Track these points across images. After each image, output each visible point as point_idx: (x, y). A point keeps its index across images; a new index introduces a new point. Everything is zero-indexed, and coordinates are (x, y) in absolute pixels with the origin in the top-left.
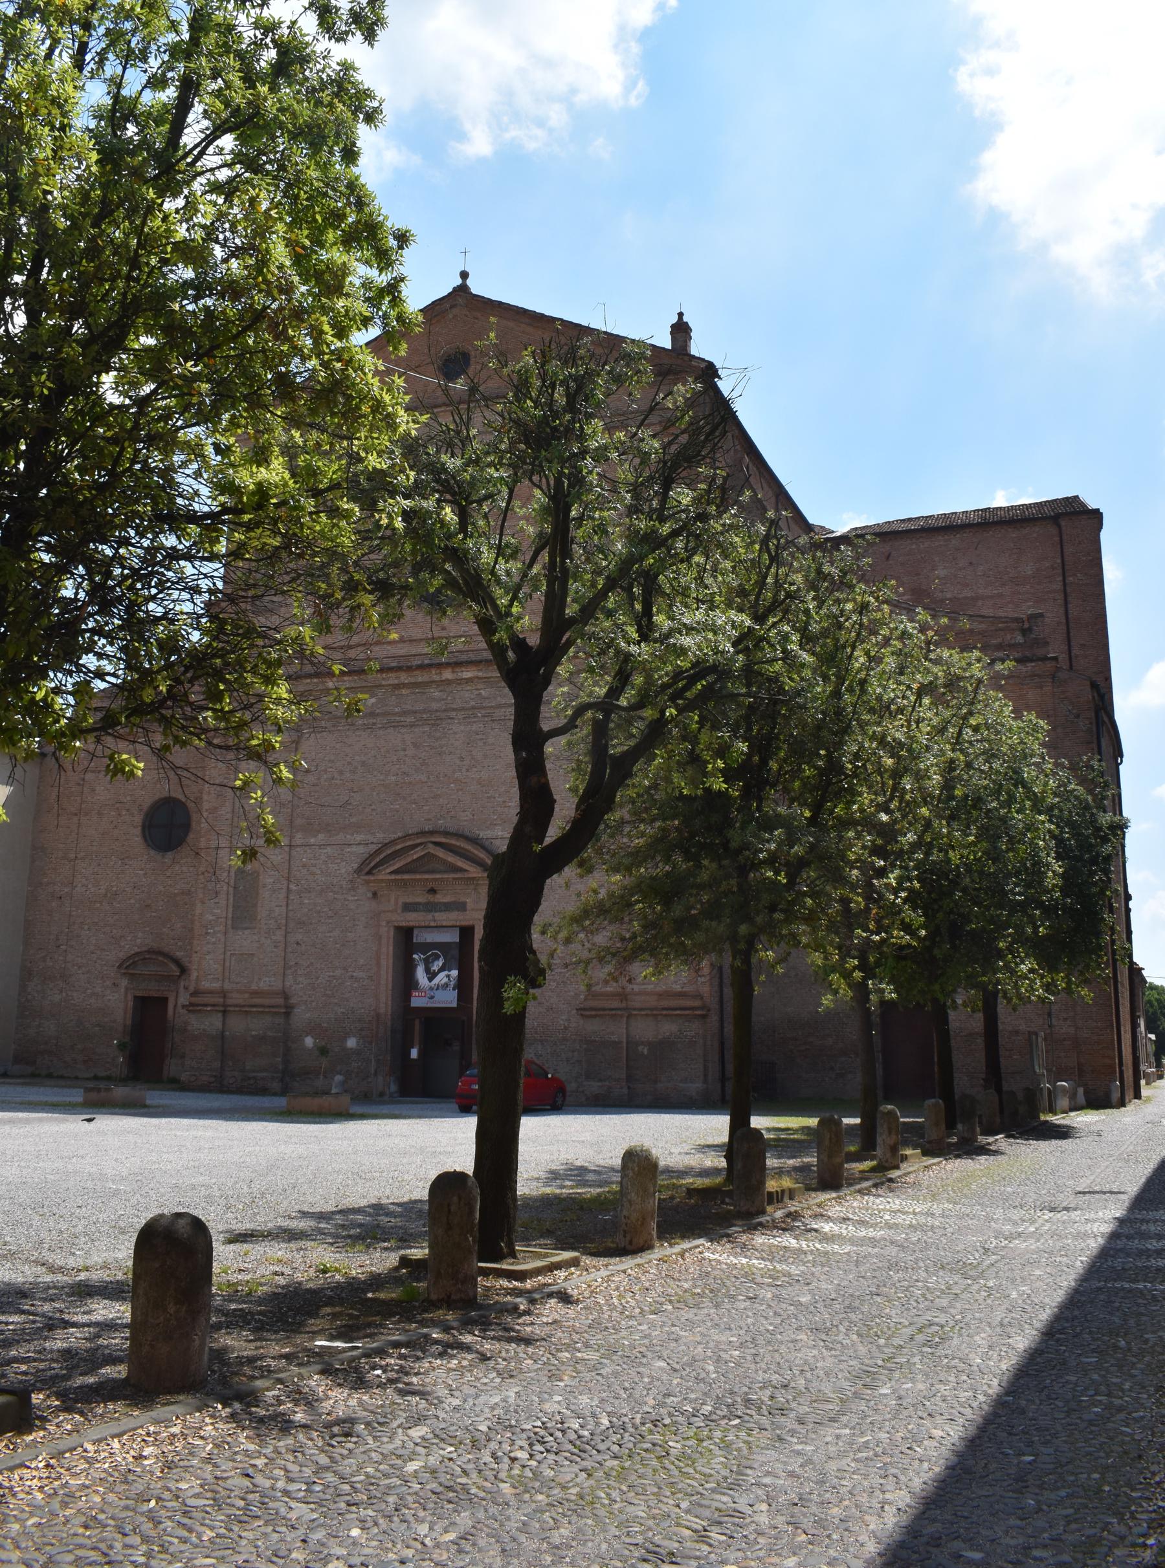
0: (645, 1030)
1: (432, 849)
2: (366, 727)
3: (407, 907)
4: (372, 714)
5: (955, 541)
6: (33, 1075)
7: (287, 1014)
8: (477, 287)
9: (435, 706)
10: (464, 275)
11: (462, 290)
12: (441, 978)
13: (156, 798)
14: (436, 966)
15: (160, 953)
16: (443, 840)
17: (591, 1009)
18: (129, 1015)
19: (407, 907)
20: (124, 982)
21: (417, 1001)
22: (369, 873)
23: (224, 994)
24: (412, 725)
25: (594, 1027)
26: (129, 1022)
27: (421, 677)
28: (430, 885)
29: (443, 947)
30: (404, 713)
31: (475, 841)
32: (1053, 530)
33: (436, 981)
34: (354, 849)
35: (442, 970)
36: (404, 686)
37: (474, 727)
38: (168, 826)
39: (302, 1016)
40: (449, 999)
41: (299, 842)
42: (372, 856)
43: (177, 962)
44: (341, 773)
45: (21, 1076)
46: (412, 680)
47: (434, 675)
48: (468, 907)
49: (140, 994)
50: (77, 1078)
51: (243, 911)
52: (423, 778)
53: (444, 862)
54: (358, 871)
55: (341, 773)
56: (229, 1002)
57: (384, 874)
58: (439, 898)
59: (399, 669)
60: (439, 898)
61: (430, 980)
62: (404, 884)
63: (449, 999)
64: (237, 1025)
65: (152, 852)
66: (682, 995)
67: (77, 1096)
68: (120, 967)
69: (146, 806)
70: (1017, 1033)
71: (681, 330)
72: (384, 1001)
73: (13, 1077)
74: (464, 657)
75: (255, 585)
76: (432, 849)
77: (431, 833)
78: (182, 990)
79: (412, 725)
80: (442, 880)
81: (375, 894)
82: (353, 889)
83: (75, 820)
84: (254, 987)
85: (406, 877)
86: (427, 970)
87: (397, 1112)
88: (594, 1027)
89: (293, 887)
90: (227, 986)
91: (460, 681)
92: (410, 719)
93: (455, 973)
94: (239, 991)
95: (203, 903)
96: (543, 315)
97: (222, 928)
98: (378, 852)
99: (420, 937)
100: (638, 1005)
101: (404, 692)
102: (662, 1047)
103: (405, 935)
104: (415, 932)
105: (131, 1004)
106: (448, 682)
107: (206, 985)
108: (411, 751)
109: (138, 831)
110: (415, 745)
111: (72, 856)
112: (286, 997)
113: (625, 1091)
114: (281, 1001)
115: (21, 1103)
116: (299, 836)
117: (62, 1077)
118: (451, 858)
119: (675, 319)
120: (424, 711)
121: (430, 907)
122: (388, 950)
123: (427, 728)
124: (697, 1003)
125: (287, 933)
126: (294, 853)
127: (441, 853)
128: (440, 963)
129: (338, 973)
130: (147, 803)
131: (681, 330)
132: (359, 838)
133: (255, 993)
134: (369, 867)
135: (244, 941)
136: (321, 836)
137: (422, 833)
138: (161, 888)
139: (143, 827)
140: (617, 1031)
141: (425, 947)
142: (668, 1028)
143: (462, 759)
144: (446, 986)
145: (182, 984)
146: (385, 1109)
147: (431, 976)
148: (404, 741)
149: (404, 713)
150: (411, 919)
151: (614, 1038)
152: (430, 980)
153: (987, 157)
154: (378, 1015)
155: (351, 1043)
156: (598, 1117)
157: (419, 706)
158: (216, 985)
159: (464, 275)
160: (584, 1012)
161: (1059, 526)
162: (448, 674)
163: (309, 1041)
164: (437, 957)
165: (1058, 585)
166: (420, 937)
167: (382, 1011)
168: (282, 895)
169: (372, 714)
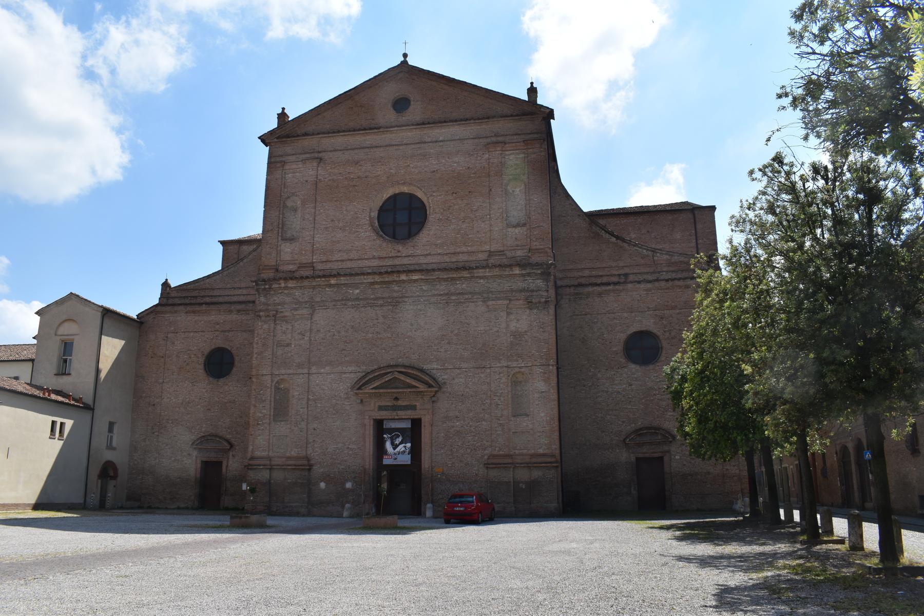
0: (523, 475)
1: (397, 375)
2: (353, 307)
3: (381, 408)
4: (357, 299)
5: (640, 220)
6: (139, 507)
7: (309, 470)
8: (411, 61)
9: (395, 295)
10: (405, 55)
11: (404, 63)
12: (401, 448)
13: (213, 347)
14: (397, 442)
15: (216, 436)
16: (403, 370)
17: (493, 464)
18: (199, 470)
19: (381, 408)
20: (195, 453)
21: (387, 461)
22: (359, 388)
23: (269, 458)
24: (381, 306)
25: (494, 474)
26: (198, 476)
27: (387, 278)
28: (395, 395)
29: (402, 431)
30: (377, 299)
31: (422, 370)
32: (690, 216)
33: (398, 449)
34: (348, 375)
35: (401, 443)
36: (377, 283)
37: (419, 307)
38: (219, 364)
39: (318, 470)
40: (406, 459)
41: (314, 371)
42: (361, 379)
43: (228, 441)
44: (339, 332)
45: (132, 508)
46: (381, 280)
47: (395, 277)
48: (418, 407)
49: (204, 459)
50: (166, 508)
51: (281, 410)
52: (389, 335)
53: (404, 382)
54: (352, 388)
55: (339, 332)
56: (273, 463)
57: (368, 389)
58: (400, 403)
59: (374, 273)
61: (394, 449)
62: (380, 396)
63: (406, 459)
64: (278, 476)
65: (211, 379)
66: (543, 455)
67: (226, 520)
68: (193, 444)
69: (206, 352)
70: (709, 473)
71: (532, 91)
72: (368, 461)
73: (127, 509)
74: (412, 268)
75: (338, 242)
76: (397, 375)
77: (396, 366)
78: (231, 456)
79: (381, 306)
80: (403, 392)
81: (362, 401)
82: (348, 398)
83: (162, 360)
84: (288, 454)
85: (381, 391)
86: (392, 444)
87: (418, 525)
88: (494, 474)
89: (311, 397)
90: (271, 454)
91: (411, 281)
92: (381, 302)
93: (409, 445)
94: (279, 457)
95: (255, 406)
96: (454, 79)
97: (267, 421)
98: (363, 377)
99: (387, 425)
100: (519, 461)
101: (376, 286)
102: (533, 485)
103: (379, 424)
104: (385, 422)
105: (199, 466)
106: (404, 281)
107: (258, 454)
108: (381, 320)
109: (202, 367)
110: (383, 316)
111: (161, 381)
112: (309, 460)
113: (513, 509)
114: (305, 462)
115: (191, 526)
116: (314, 368)
117: (158, 508)
118: (408, 380)
119: (529, 86)
120: (389, 297)
121: (395, 408)
122: (370, 432)
123: (390, 307)
124: (553, 460)
125: (308, 423)
126: (311, 378)
127: (402, 377)
128: (400, 439)
129: (340, 445)
130: (207, 351)
131: (532, 91)
132: (350, 369)
133: (289, 458)
134: (360, 385)
135: (281, 428)
136: (327, 368)
137: (389, 366)
138: (216, 399)
139: (205, 365)
140: (507, 476)
141: (390, 431)
142: (537, 474)
143: (412, 325)
144: (404, 452)
145: (231, 453)
146: (294, 522)
147: (395, 447)
148: (377, 314)
149: (377, 299)
150: (383, 415)
151: (506, 480)
152: (394, 449)
153: (536, 56)
154: (365, 469)
155: (349, 485)
156: (538, 523)
157: (386, 295)
158: (264, 454)
159: (405, 55)
160: (487, 466)
161: (694, 214)
162: (403, 277)
163: (323, 485)
164: (398, 436)
165: (694, 244)
166: (387, 425)
167: (367, 467)
168: (304, 402)
169: (357, 299)
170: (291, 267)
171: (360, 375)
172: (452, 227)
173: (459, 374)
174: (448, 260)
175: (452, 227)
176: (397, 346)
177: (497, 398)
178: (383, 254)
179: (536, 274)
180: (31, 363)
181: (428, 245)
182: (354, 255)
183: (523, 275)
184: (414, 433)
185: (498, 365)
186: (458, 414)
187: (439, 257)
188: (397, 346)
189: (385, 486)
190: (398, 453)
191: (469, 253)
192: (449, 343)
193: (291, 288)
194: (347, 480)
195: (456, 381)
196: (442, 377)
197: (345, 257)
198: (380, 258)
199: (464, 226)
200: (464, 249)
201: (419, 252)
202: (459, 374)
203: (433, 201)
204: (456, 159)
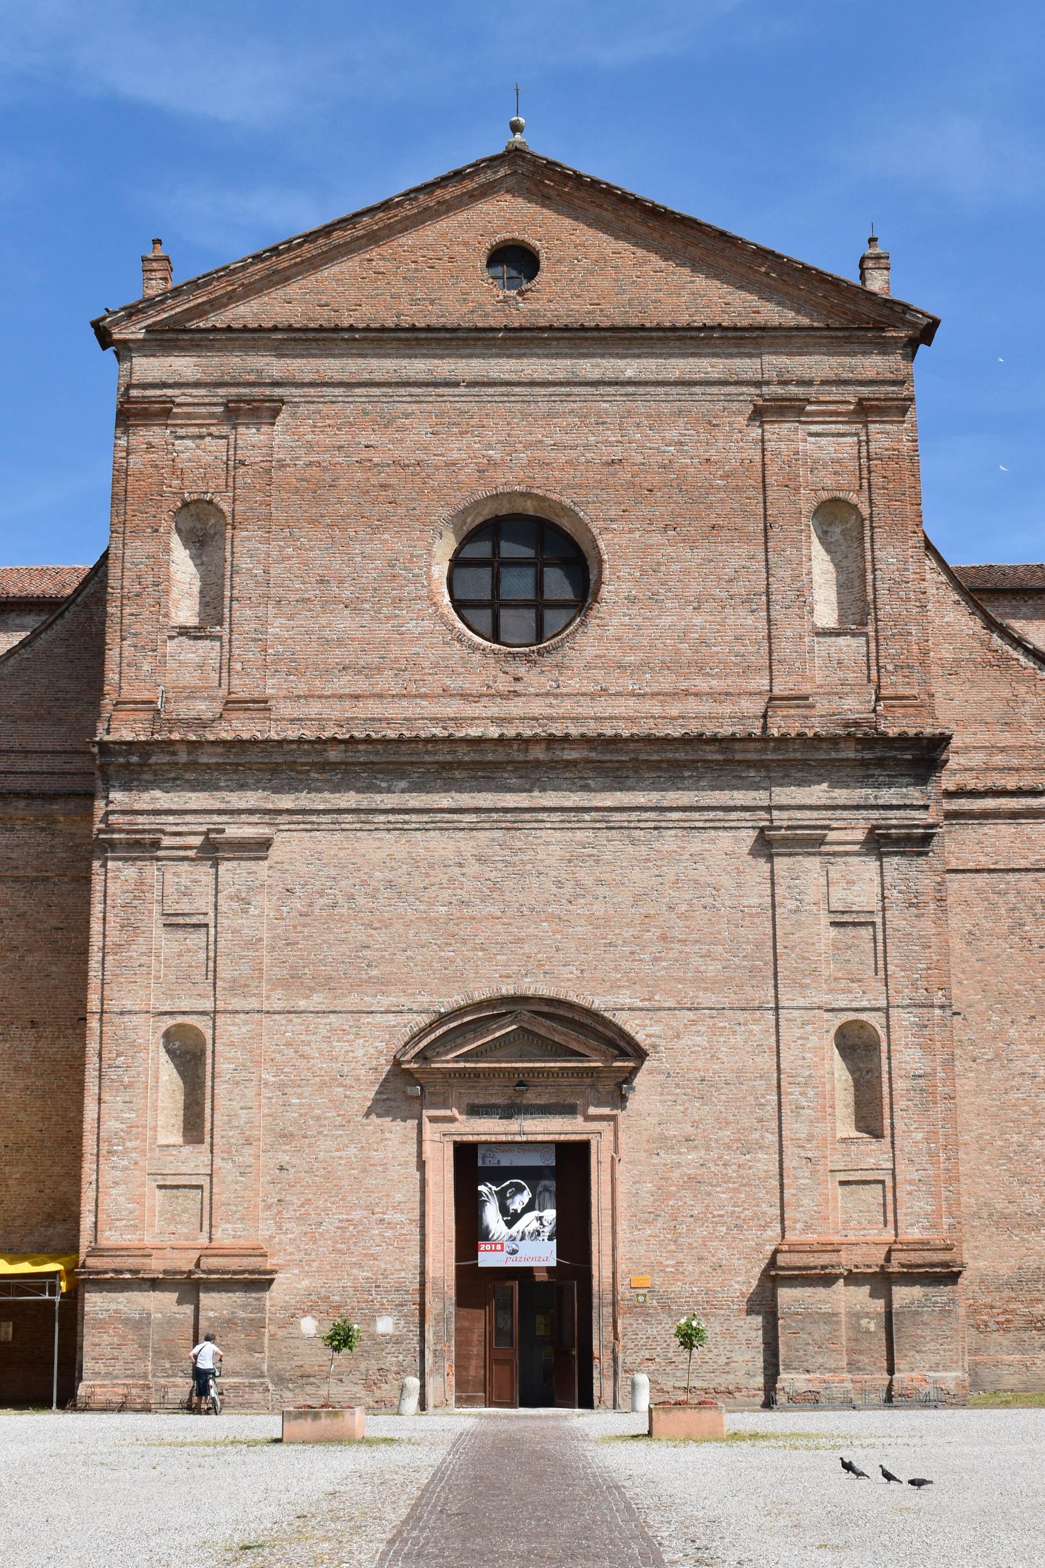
12: (528, 1222)
14: (518, 1202)
21: (487, 1259)
29: (531, 1175)
33: (519, 1226)
35: (529, 1208)
36: (460, 765)
40: (542, 1254)
46: (477, 757)
55: (351, 897)
60: (531, 1098)
61: (510, 1224)
63: (542, 1254)
86: (504, 1210)
93: (550, 1214)
98: (431, 1027)
101: (457, 774)
104: (481, 1151)
128: (525, 1197)
143: (559, 884)
147: (512, 1218)
152: (510, 1224)
164: (520, 1190)
170: (202, 708)
171: (424, 1020)
172: (666, 621)
173: (694, 1022)
174: (657, 711)
175: (666, 621)
176: (519, 941)
177: (797, 1090)
178: (473, 684)
179: (898, 762)
180: (880, 1186)
181: (609, 671)
182: (386, 682)
183: (864, 763)
184: (566, 1176)
185: (801, 1002)
186: (689, 1129)
187: (632, 702)
188: (519, 941)
189: (128, 1276)
190: (522, 1238)
191: (715, 696)
192: (664, 938)
193: (208, 766)
194: (382, 1310)
195: (685, 1041)
196: (639, 1028)
197: (362, 685)
198: (464, 696)
199: (698, 620)
200: (702, 684)
201: (574, 684)
202: (694, 1022)
203: (615, 545)
204: (672, 434)
